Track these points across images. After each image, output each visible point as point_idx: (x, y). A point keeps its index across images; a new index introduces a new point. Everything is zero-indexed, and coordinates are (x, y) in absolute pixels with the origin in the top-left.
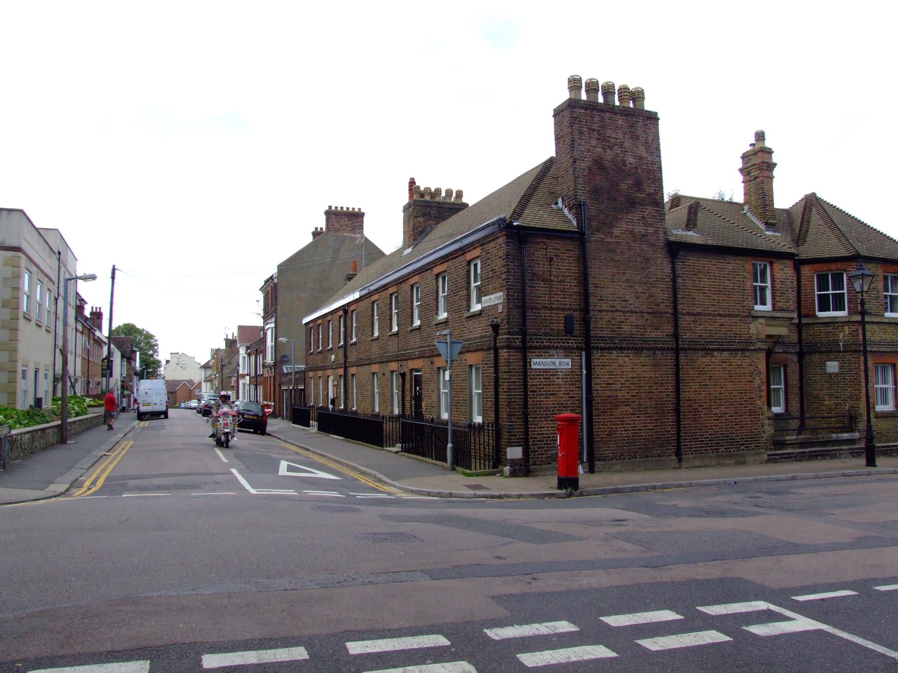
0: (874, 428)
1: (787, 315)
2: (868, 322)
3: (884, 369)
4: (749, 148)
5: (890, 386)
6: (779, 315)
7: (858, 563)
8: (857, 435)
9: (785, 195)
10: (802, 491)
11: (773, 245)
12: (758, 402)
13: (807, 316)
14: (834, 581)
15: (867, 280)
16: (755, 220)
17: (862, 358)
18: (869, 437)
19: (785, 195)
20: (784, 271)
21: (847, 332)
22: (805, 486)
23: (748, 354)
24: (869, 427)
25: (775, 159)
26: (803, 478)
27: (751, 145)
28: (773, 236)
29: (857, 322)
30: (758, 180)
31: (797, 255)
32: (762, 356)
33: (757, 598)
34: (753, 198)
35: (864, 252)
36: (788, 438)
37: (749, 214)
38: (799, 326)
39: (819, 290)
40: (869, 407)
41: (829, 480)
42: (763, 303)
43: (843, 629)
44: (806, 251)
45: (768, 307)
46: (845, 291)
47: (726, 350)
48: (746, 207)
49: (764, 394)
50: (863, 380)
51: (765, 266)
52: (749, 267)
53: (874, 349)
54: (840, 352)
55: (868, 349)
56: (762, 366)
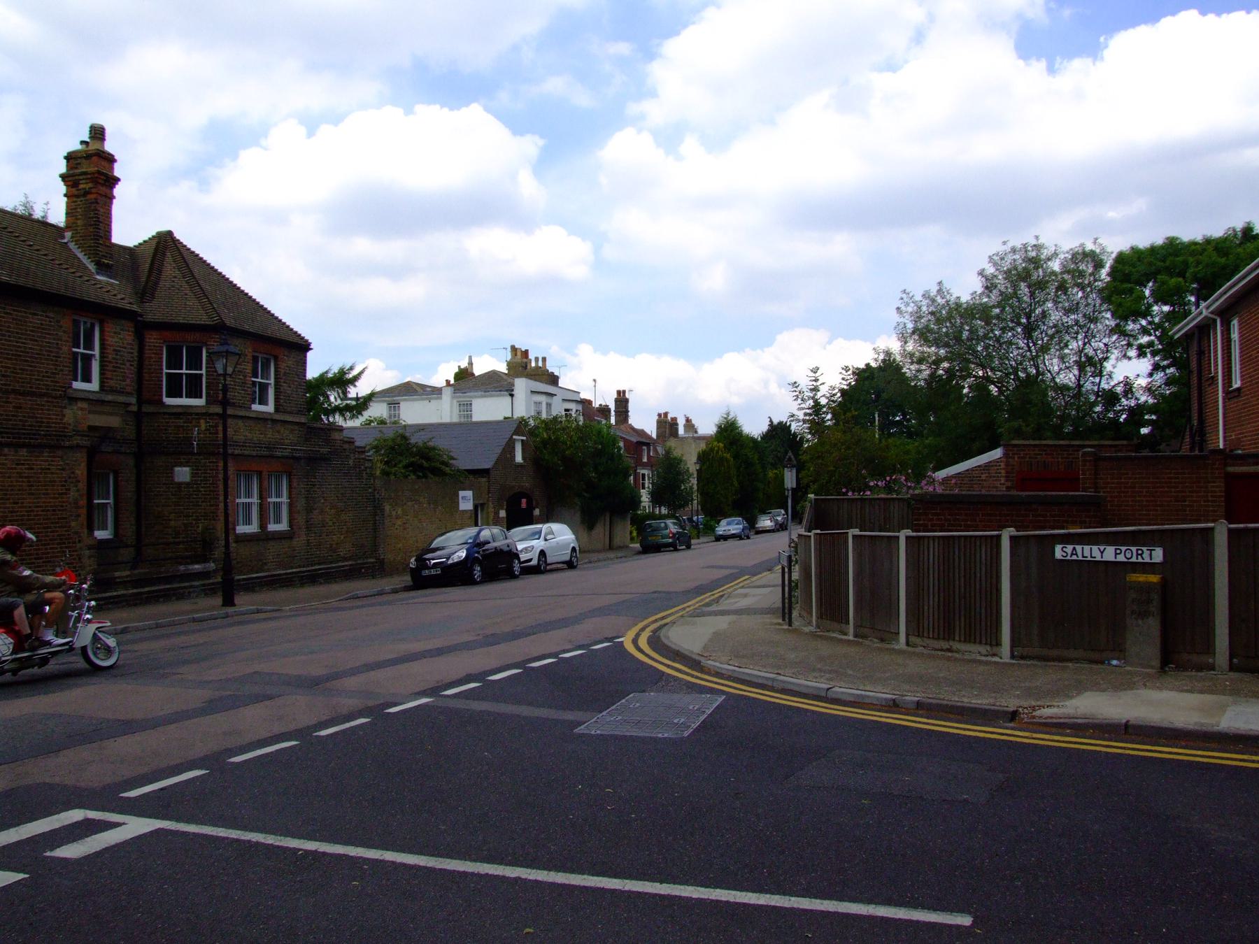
0: (233, 555)
1: (121, 399)
2: (230, 416)
3: (248, 479)
4: (78, 147)
5: (284, 499)
6: (109, 398)
7: (207, 734)
8: (212, 566)
9: (130, 226)
10: (136, 647)
11: (106, 296)
12: (73, 524)
13: (150, 402)
14: (179, 761)
15: (234, 359)
16: (80, 255)
17: (221, 464)
18: (228, 568)
19: (130, 226)
20: (122, 337)
21: (203, 427)
22: (142, 640)
23: (60, 453)
24: (227, 554)
25: (118, 171)
26: (137, 629)
27: (82, 142)
28: (108, 283)
29: (217, 414)
30: (89, 197)
31: (141, 316)
32: (81, 457)
33: (68, 806)
34: (80, 222)
35: (229, 322)
36: (117, 574)
37: (72, 246)
38: (139, 417)
39: (168, 368)
40: (229, 528)
41: (212, 623)
42: (87, 379)
43: (188, 821)
44: (155, 311)
45: (94, 386)
46: (204, 372)
47: (24, 446)
48: (68, 235)
49: (84, 511)
50: (221, 492)
51: (93, 326)
52: (66, 323)
53: (236, 452)
54: (193, 454)
55: (230, 451)
56: (81, 471)
